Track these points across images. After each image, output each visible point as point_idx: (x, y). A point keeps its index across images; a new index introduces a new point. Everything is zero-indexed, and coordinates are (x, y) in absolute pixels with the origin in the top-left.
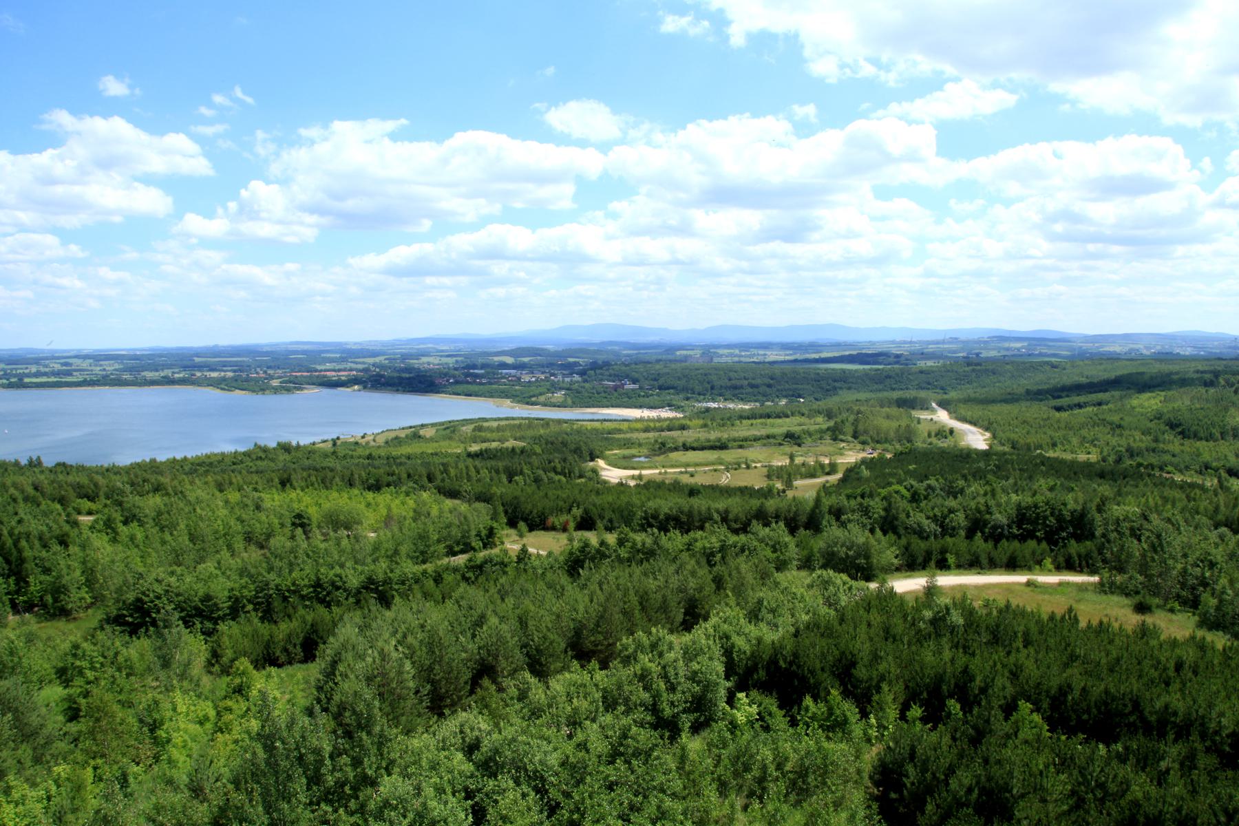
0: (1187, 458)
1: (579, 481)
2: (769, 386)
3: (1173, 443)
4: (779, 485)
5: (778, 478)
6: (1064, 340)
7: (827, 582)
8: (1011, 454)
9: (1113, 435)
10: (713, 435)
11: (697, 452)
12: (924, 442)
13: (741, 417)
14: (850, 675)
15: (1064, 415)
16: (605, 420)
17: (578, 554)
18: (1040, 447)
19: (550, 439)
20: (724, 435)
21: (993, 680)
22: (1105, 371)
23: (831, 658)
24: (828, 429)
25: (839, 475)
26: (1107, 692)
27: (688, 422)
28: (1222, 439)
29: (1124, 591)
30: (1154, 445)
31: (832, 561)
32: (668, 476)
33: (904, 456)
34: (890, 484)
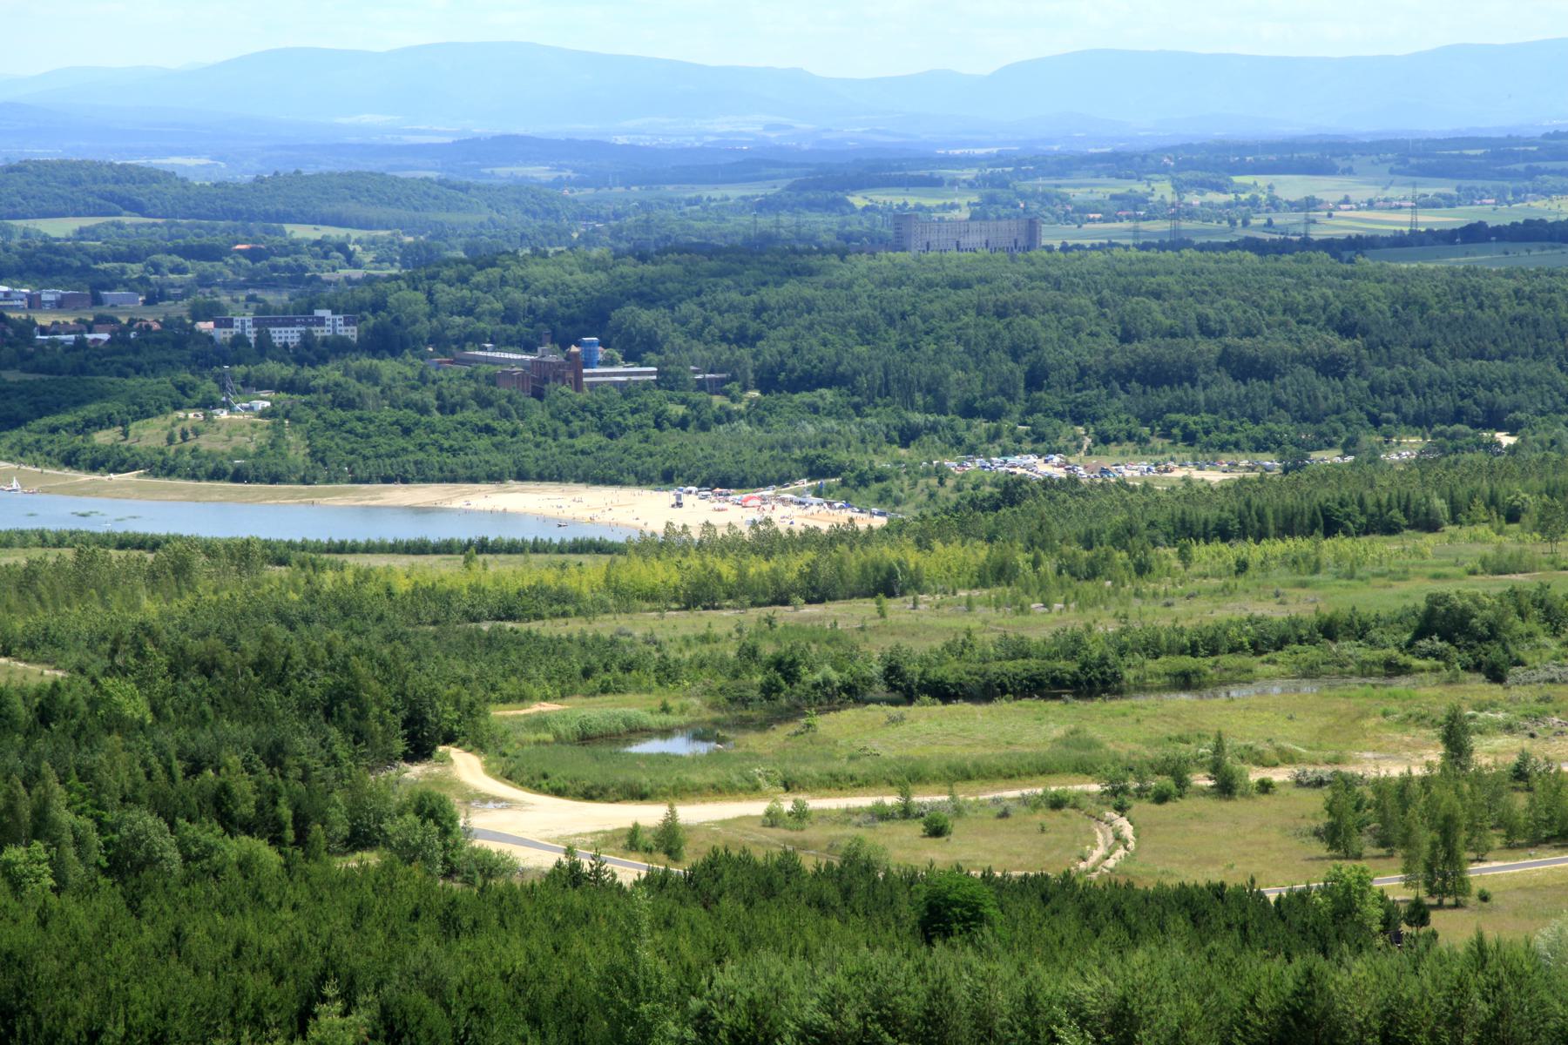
1: (352, 862)
2: (1331, 367)
11: (961, 708)
13: (1185, 531)
16: (484, 547)
19: (196, 647)
27: (913, 558)
32: (812, 833)
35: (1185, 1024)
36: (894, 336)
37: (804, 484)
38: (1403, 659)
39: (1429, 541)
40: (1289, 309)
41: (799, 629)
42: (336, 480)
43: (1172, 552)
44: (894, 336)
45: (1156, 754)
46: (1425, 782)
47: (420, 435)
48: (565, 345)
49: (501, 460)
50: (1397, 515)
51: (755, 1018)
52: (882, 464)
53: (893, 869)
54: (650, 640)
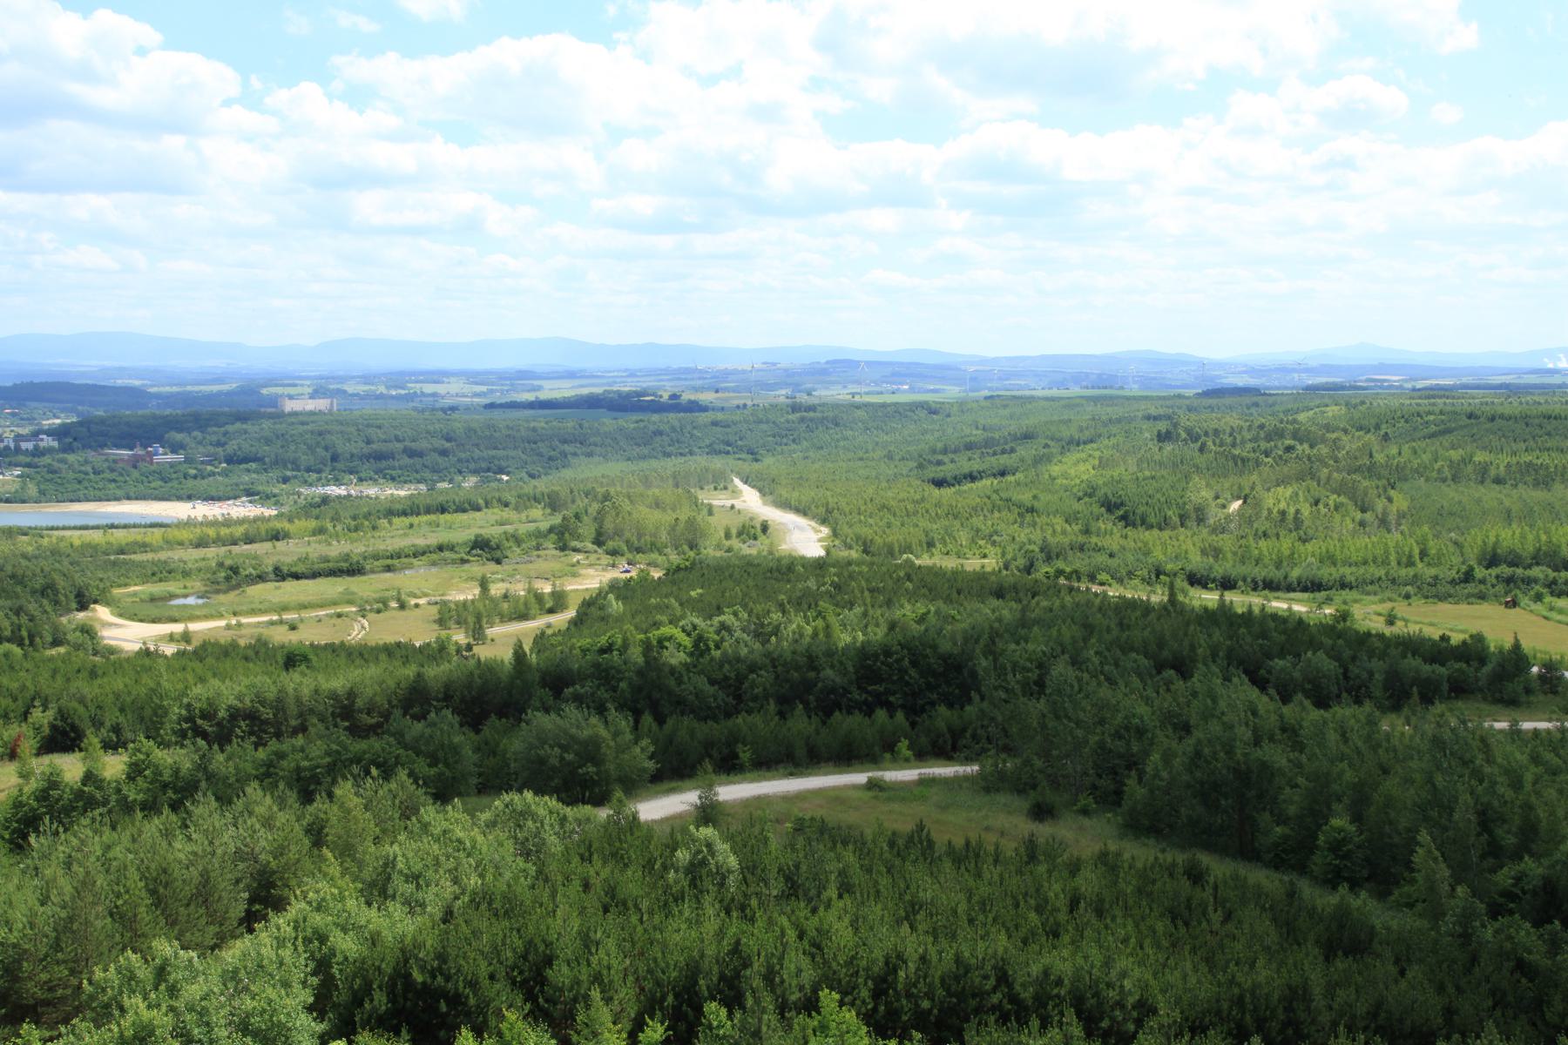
0: (1130, 558)
1: (53, 652)
2: (444, 453)
3: (1112, 535)
4: (460, 637)
5: (458, 623)
6: (945, 371)
7: (522, 814)
8: (859, 564)
9: (1021, 525)
10: (336, 549)
12: (718, 547)
13: (390, 513)
14: (542, 981)
15: (947, 492)
16: (113, 526)
17: (34, 804)
18: (908, 549)
20: (356, 547)
21: (781, 958)
22: (1011, 417)
23: (509, 954)
24: (551, 530)
25: (571, 613)
26: (958, 960)
27: (287, 526)
28: (1182, 525)
29: (1021, 786)
30: (1081, 539)
31: (540, 778)
32: (244, 631)
33: (681, 574)
34: (657, 625)
35: (375, 695)
36: (279, 443)
37: (244, 499)
38: (466, 557)
39: (478, 514)
40: (428, 432)
41: (242, 555)
42: (50, 501)
43: (385, 521)
44: (279, 443)
45: (377, 596)
46: (473, 601)
47: (86, 484)
48: (146, 447)
49: (119, 493)
50: (466, 505)
51: (210, 705)
52: (276, 491)
53: (483, 659)
54: (181, 560)
